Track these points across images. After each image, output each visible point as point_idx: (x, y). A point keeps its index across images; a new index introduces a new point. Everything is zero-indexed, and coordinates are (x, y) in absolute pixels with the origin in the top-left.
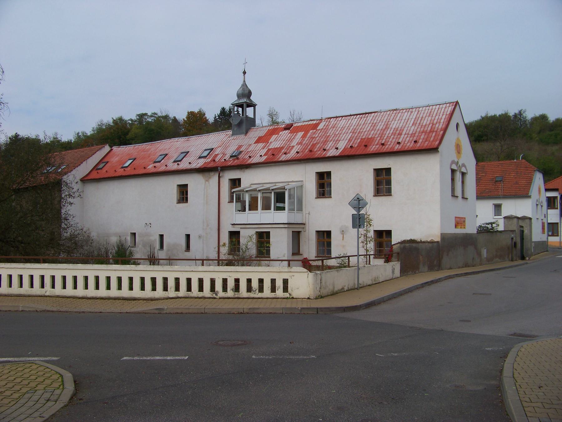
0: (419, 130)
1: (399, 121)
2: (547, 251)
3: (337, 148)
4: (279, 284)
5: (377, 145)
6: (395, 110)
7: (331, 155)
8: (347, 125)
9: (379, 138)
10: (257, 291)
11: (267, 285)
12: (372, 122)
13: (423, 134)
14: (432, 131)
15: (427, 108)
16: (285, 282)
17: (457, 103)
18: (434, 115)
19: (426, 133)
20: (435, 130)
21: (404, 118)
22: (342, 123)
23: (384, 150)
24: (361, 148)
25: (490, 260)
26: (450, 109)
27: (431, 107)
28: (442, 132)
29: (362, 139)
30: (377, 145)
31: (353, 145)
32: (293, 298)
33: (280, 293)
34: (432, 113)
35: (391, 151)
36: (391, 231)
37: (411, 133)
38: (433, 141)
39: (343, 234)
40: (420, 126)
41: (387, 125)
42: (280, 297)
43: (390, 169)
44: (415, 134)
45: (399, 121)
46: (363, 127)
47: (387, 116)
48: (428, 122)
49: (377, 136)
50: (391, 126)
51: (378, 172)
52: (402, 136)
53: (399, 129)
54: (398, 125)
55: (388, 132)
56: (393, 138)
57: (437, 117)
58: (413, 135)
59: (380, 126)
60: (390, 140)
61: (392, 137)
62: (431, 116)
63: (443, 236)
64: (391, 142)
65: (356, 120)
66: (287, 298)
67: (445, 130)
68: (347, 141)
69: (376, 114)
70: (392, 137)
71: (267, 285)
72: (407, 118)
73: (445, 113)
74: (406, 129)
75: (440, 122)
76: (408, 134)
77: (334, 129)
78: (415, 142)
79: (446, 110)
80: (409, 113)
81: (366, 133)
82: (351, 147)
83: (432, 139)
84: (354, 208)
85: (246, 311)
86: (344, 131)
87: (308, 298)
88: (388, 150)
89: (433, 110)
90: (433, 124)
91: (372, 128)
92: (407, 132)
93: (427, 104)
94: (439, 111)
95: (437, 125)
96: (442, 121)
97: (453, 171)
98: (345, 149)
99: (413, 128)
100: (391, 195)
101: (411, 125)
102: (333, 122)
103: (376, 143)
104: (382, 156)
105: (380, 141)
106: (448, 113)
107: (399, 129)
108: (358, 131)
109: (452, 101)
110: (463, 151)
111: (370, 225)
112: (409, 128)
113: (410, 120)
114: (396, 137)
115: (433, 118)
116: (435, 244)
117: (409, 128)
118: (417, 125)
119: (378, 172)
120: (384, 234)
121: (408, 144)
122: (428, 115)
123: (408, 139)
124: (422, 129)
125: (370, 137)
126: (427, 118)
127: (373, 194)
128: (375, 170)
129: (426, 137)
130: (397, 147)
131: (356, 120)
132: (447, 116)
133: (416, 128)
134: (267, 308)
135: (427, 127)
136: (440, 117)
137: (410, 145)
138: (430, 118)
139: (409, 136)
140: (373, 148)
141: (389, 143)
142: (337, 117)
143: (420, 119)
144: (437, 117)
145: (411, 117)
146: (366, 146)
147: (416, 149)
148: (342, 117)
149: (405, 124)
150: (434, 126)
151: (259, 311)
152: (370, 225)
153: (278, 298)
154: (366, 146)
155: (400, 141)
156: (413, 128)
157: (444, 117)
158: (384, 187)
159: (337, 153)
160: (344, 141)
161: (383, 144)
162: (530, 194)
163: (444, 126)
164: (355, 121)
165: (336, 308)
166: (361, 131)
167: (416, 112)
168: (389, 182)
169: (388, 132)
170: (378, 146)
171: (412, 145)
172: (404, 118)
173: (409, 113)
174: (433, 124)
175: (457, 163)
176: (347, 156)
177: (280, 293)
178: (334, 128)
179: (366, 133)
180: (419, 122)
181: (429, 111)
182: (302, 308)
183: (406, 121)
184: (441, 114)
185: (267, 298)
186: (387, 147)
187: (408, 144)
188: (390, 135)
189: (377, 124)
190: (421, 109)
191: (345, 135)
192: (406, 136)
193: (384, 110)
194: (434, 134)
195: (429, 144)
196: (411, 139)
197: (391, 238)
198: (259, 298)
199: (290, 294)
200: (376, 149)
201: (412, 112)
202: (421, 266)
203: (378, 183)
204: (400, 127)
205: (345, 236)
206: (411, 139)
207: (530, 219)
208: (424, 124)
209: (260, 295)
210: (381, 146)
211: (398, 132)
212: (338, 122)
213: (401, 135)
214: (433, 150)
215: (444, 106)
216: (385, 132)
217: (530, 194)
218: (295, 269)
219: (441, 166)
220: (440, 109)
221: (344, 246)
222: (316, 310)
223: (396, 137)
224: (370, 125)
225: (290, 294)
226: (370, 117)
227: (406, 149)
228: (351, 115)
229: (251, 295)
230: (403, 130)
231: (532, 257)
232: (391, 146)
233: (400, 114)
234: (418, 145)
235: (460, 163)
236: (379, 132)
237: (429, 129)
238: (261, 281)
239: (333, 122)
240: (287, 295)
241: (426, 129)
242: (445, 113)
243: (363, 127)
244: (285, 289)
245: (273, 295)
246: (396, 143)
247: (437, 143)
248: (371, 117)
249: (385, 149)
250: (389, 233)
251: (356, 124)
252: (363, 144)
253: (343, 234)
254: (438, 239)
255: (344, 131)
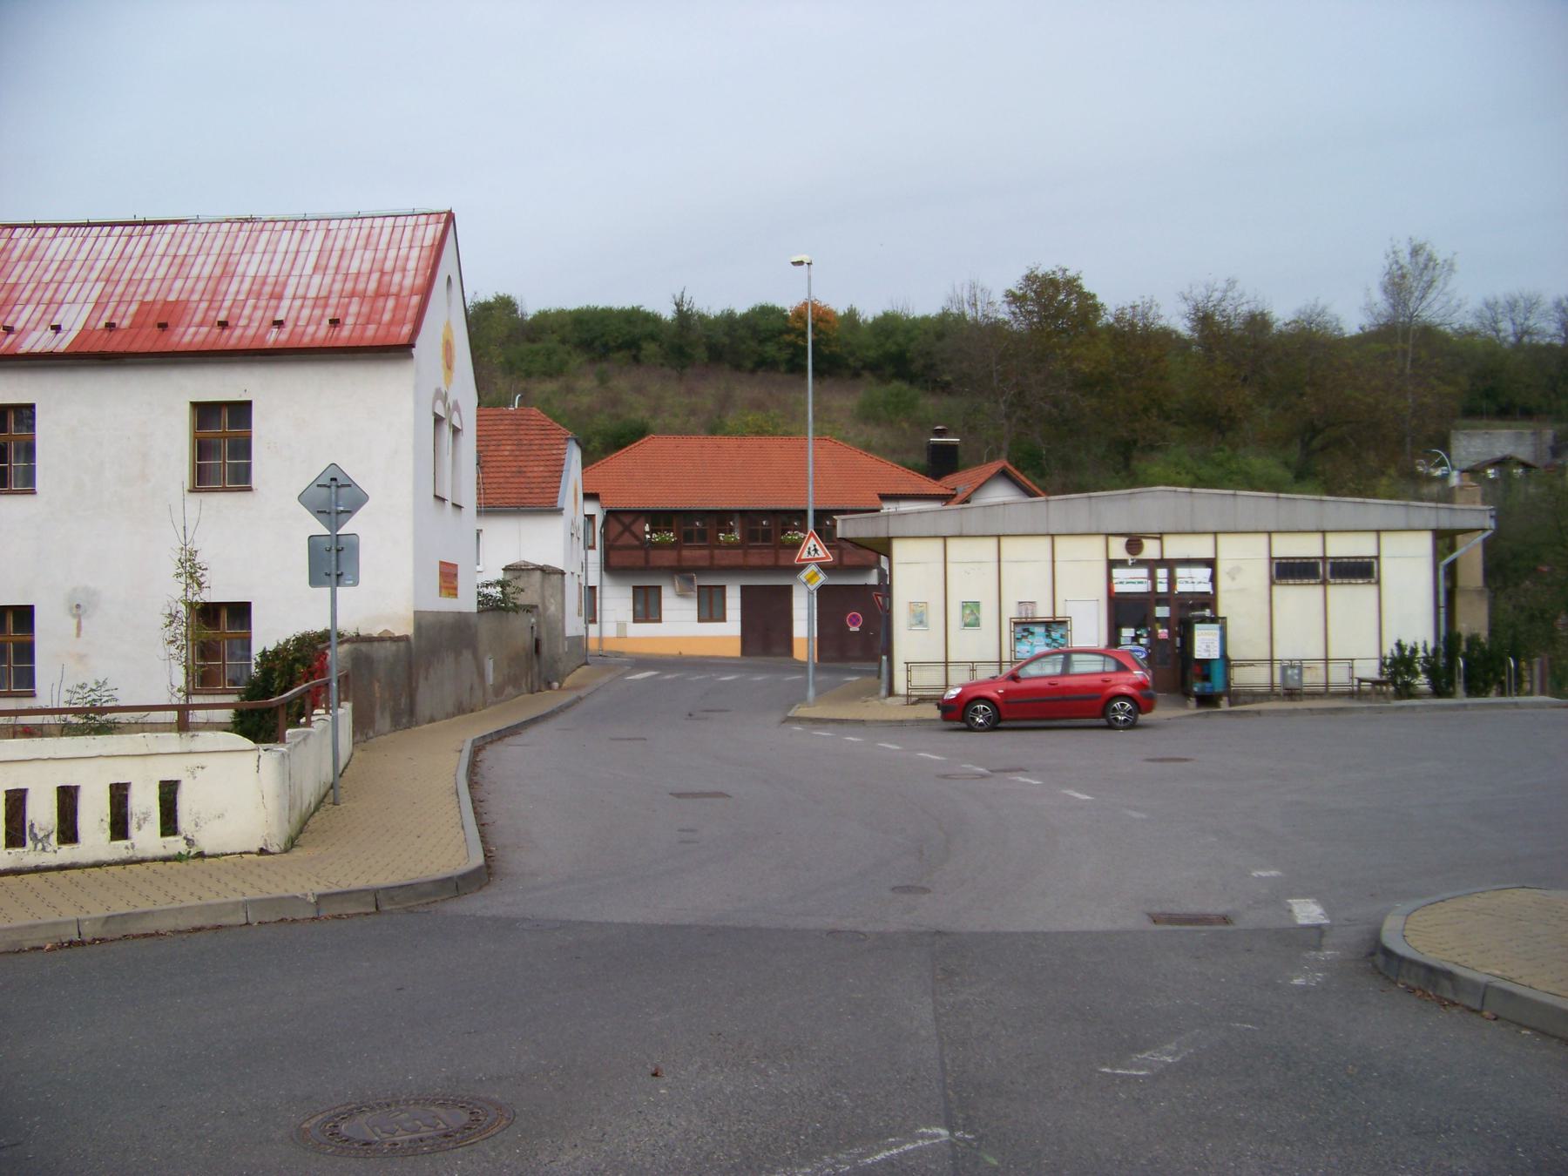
0: (337, 287)
1: (268, 257)
2: (586, 664)
3: (57, 329)
4: (145, 802)
5: (201, 324)
6: (246, 220)
7: (37, 349)
8: (82, 256)
9: (204, 305)
10: (54, 837)
11: (93, 813)
12: (172, 251)
13: (356, 300)
14: (381, 294)
15: (357, 223)
16: (169, 793)
17: (450, 217)
18: (383, 246)
19: (363, 296)
20: (394, 289)
21: (282, 247)
22: (62, 245)
23: (232, 343)
24: (146, 331)
25: (498, 690)
26: (432, 232)
27: (367, 222)
28: (415, 300)
29: (142, 303)
30: (201, 324)
31: (116, 321)
32: (201, 855)
33: (146, 837)
34: (374, 240)
35: (255, 346)
36: (248, 604)
37: (312, 293)
38: (392, 322)
39: (78, 617)
40: (340, 277)
41: (226, 264)
42: (149, 855)
43: (247, 405)
44: (328, 297)
45: (268, 257)
46: (143, 265)
47: (221, 236)
48: (366, 267)
49: (196, 297)
50: (241, 269)
51: (204, 412)
52: (286, 303)
53: (271, 280)
54: (264, 268)
55: (233, 288)
56: (255, 308)
57: (392, 253)
58: (322, 301)
59: (204, 267)
60: (247, 312)
61: (251, 302)
62: (372, 247)
63: (419, 616)
64: (250, 319)
65: (112, 240)
66: (178, 858)
67: (426, 292)
68: (89, 307)
69: (182, 228)
70: (251, 302)
71: (93, 813)
72: (293, 248)
73: (417, 243)
74: (293, 281)
75: (404, 270)
76: (304, 298)
77: (33, 264)
78: (335, 322)
79: (419, 233)
80: (298, 234)
81: (155, 285)
82: (110, 326)
83: (387, 317)
84: (319, 513)
85: (89, 932)
86: (73, 273)
87: (262, 852)
88: (245, 345)
89: (377, 231)
90: (383, 273)
91: (174, 270)
92: (301, 292)
93: (353, 211)
94: (397, 236)
95: (397, 277)
96: (412, 265)
97: (438, 420)
98: (85, 333)
99: (317, 279)
100: (250, 489)
101: (308, 270)
102: (23, 242)
103: (198, 318)
104: (219, 363)
105: (212, 314)
106: (428, 242)
107: (271, 280)
108: (126, 276)
109: (435, 209)
110: (456, 364)
111: (200, 585)
112: (304, 281)
113: (302, 256)
114: (263, 303)
115: (380, 255)
116: (402, 644)
117: (304, 281)
118: (331, 271)
119: (204, 412)
120: (224, 615)
121: (311, 329)
122: (361, 243)
123: (306, 313)
124: (349, 286)
125: (172, 298)
126: (358, 253)
127: (187, 486)
128: (195, 405)
129: (365, 309)
130: (273, 338)
131: (112, 240)
132: (425, 253)
133: (328, 280)
134: (181, 910)
135: (363, 279)
136: (403, 252)
137: (319, 333)
138: (369, 255)
139: (309, 303)
140: (189, 335)
141: (243, 322)
142: (37, 226)
143: (336, 254)
144: (392, 253)
145: (305, 247)
146: (163, 326)
147: (339, 344)
148: (59, 226)
149: (287, 266)
150: (386, 278)
151: (149, 926)
152: (200, 585)
153: (142, 861)
154: (163, 326)
155: (280, 316)
156: (317, 279)
157: (415, 253)
158: (223, 462)
159: (63, 343)
160: (77, 307)
161: (224, 325)
162: (559, 505)
163: (420, 281)
164: (109, 244)
165: (435, 882)
166: (138, 276)
167: (321, 234)
168: (243, 448)
169: (233, 288)
170: (205, 330)
171: (322, 333)
172: (282, 247)
173: (298, 234)
174: (383, 273)
175: (445, 399)
176: (93, 356)
177: (146, 837)
178: (30, 259)
179: (155, 285)
180: (334, 262)
181: (365, 232)
182: (322, 898)
183: (290, 256)
184: (405, 244)
185: (98, 865)
186: (238, 332)
187: (311, 329)
188: (242, 297)
189: (190, 260)
190: (334, 224)
191: (77, 286)
192: (298, 303)
193: (211, 219)
194: (391, 303)
195: (382, 332)
196: (318, 312)
197: (249, 627)
198: (61, 868)
199: (190, 842)
200: (200, 338)
201: (305, 231)
202: (377, 714)
203: (202, 449)
204: (274, 272)
205: (84, 623)
206: (318, 312)
207: (563, 573)
208: (354, 270)
209: (67, 854)
210: (217, 330)
211: (268, 289)
212: (45, 243)
213: (280, 297)
214: (399, 350)
215: (411, 221)
216: (223, 288)
217: (559, 505)
218: (207, 739)
219: (417, 403)
220: (398, 232)
221: (81, 658)
222: (371, 899)
223: (263, 303)
224: (167, 260)
225: (190, 842)
226: (163, 237)
227: (306, 341)
228: (89, 225)
229: (27, 856)
230: (285, 285)
231: (568, 681)
232: (251, 332)
233: (265, 235)
234: (345, 332)
235: (450, 401)
236: (201, 286)
237: (373, 285)
238: (68, 798)
239: (23, 242)
240: (176, 845)
241: (361, 286)
242: (417, 243)
243: (143, 265)
244: (169, 824)
245: (120, 849)
246: (267, 323)
247: (407, 329)
248: (167, 238)
249: (232, 339)
250: (241, 612)
251: (116, 255)
252: (152, 320)
253: (78, 617)
254: (405, 628)
255: (73, 273)
